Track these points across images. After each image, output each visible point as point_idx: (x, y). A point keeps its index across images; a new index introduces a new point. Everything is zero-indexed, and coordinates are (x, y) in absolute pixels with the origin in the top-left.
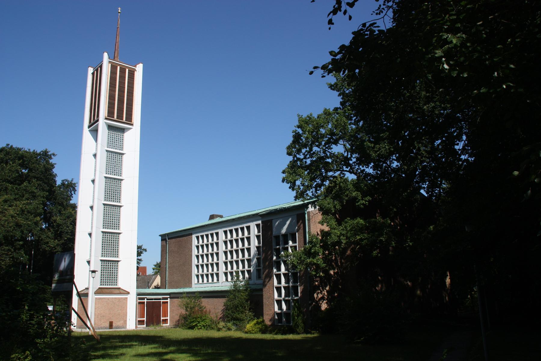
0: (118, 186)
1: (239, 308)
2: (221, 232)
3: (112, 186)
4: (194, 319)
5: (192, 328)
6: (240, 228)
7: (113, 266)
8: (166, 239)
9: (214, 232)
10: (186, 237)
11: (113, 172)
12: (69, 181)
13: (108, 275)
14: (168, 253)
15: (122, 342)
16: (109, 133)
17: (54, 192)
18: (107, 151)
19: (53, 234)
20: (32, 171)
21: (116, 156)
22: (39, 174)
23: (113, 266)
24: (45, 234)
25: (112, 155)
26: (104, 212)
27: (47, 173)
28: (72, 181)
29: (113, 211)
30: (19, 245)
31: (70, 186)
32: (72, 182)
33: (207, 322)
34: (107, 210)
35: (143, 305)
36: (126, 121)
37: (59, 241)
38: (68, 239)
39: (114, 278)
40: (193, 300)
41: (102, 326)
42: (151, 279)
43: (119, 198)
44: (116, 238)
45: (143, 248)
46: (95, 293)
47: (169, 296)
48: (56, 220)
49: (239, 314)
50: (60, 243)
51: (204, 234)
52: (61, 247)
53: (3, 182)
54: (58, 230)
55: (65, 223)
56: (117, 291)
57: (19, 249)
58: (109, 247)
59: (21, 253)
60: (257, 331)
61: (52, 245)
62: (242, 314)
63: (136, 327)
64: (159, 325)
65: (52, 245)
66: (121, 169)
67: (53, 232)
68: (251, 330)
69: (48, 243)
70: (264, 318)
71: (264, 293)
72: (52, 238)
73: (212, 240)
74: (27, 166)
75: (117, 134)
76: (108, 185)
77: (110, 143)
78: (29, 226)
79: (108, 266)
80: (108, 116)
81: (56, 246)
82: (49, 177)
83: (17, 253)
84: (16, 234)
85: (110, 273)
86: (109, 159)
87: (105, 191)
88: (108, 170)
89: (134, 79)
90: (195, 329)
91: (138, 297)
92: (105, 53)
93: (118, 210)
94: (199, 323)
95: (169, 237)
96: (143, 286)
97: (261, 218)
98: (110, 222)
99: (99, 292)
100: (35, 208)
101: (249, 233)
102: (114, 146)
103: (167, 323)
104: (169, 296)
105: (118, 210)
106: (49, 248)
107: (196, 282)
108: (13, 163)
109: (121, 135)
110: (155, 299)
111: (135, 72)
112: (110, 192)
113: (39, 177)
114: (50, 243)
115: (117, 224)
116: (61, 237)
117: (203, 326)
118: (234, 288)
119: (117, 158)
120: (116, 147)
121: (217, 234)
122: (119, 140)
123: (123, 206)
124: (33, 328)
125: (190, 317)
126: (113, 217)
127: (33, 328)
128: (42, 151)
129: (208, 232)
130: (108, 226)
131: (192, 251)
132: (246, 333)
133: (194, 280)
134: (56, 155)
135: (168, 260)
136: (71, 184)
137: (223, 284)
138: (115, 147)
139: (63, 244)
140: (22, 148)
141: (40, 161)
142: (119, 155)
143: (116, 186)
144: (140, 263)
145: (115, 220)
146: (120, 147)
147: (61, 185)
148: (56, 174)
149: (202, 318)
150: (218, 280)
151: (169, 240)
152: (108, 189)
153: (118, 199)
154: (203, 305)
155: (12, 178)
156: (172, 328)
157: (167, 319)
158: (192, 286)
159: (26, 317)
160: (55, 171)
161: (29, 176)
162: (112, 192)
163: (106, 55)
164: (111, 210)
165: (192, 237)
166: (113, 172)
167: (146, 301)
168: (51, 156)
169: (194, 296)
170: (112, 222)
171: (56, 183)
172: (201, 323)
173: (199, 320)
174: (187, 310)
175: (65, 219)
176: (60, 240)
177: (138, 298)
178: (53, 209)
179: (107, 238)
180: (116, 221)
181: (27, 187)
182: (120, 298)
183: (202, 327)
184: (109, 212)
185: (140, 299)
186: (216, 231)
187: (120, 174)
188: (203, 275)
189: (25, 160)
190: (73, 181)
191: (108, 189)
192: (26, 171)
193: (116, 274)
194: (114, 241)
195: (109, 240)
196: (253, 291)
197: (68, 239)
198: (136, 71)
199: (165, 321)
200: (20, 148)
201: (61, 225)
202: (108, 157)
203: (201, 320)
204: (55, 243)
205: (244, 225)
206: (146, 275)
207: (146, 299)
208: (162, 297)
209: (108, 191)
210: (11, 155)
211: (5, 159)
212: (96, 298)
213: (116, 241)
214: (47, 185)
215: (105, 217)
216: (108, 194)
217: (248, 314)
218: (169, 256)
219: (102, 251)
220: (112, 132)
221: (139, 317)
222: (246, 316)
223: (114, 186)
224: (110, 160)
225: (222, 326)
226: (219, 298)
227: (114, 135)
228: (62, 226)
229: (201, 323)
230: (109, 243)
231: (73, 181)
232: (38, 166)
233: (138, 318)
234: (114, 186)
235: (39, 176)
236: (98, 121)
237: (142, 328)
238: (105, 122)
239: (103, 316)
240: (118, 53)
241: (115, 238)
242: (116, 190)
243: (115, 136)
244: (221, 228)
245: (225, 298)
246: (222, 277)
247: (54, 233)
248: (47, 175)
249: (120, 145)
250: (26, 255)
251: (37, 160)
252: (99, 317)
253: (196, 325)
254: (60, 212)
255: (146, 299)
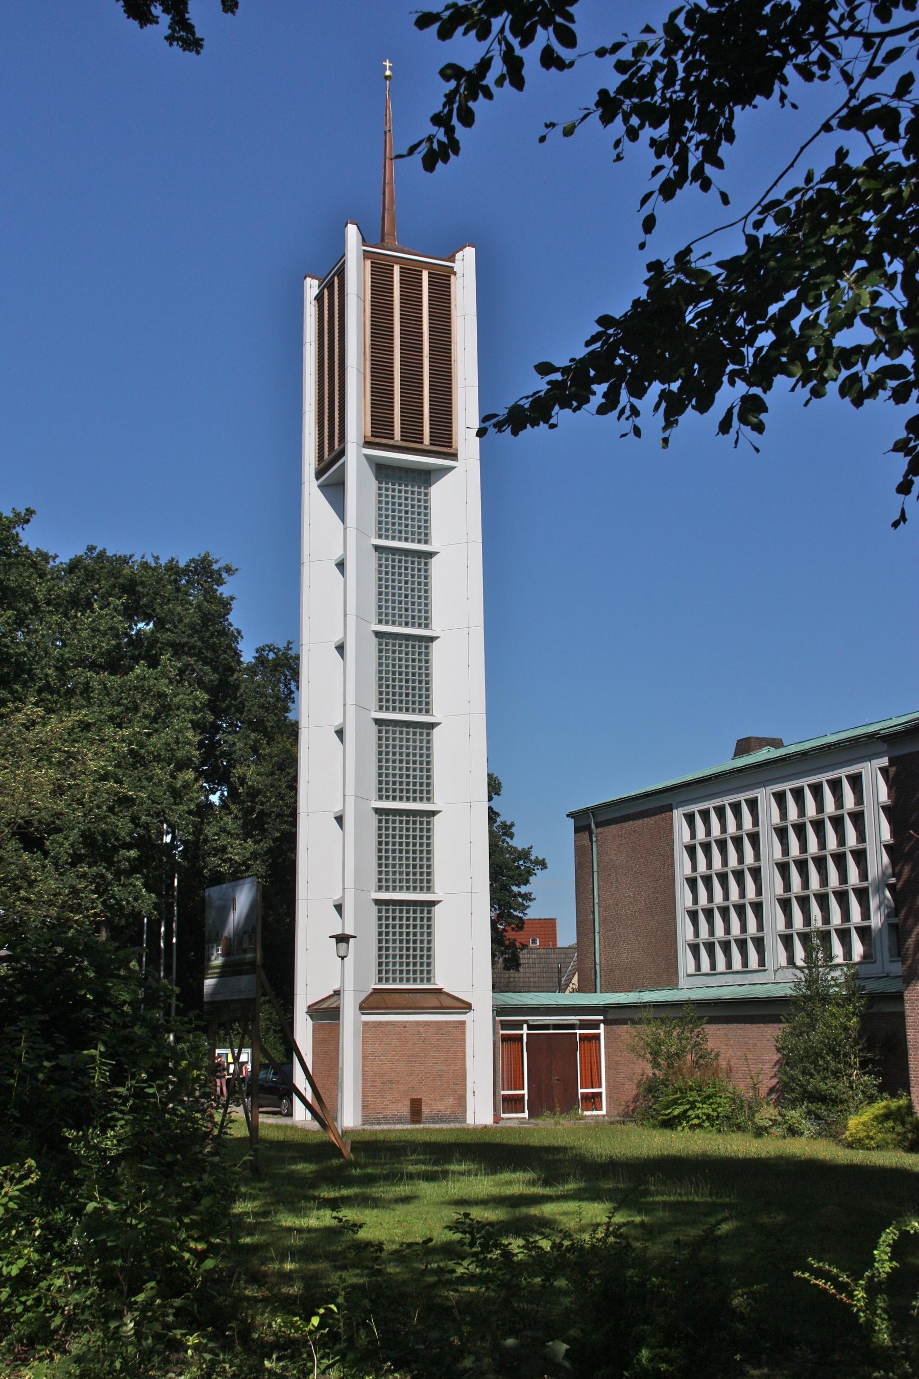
0: (420, 661)
1: (823, 1058)
2: (764, 796)
3: (400, 659)
4: (678, 1095)
5: (669, 1124)
6: (827, 781)
7: (415, 919)
8: (590, 825)
9: (741, 797)
10: (653, 818)
11: (400, 616)
12: (279, 650)
13: (401, 949)
14: (598, 871)
15: (436, 1163)
16: (380, 489)
17: (237, 687)
18: (377, 548)
19: (240, 822)
20: (163, 627)
21: (406, 562)
22: (184, 633)
23: (415, 919)
24: (214, 822)
25: (393, 560)
26: (380, 746)
27: (208, 630)
28: (288, 648)
29: (408, 740)
30: (128, 859)
31: (283, 666)
32: (290, 652)
33: (720, 1105)
34: (387, 739)
35: (516, 1045)
36: (431, 444)
37: (256, 842)
38: (283, 834)
39: (422, 957)
40: (674, 1028)
41: (389, 1113)
42: (568, 960)
43: (424, 699)
44: (421, 830)
45: (533, 858)
46: (361, 1008)
47: (601, 1018)
48: (245, 775)
49: (826, 1078)
50: (262, 848)
51: (709, 805)
52: (264, 861)
53: (75, 667)
54: (252, 810)
55: (272, 786)
56: (433, 1001)
57: (129, 873)
58: (401, 859)
59: (134, 886)
60: (883, 1139)
61: (237, 857)
62: (838, 1078)
63: (497, 1119)
64: (572, 1113)
65: (237, 857)
66: (426, 605)
67: (240, 815)
68: (862, 1134)
69: (224, 849)
70: (913, 1097)
71: (907, 1006)
72: (237, 835)
73: (737, 825)
74: (149, 611)
75: (406, 492)
76: (387, 658)
77: (387, 523)
78: (154, 802)
79: (401, 919)
80: (372, 436)
81: (249, 859)
82: (214, 643)
83: (124, 885)
84: (117, 826)
85: (408, 942)
86: (387, 573)
87: (380, 679)
88: (383, 610)
89: (448, 301)
90: (679, 1128)
91: (498, 1018)
92: (349, 226)
93: (424, 737)
94: (693, 1107)
95: (600, 819)
96: (544, 984)
97: (884, 747)
98: (401, 776)
99: (375, 1005)
100: (169, 745)
101: (859, 800)
102: (400, 532)
103: (601, 1109)
104: (601, 1018)
105: (424, 737)
106: (228, 865)
107: (691, 969)
108: (101, 608)
109: (419, 493)
110: (556, 1027)
111: (453, 277)
112: (394, 680)
113: (187, 643)
114: (230, 849)
115: (421, 784)
116: (263, 831)
117: (707, 1119)
118: (808, 988)
119: (413, 569)
120: (406, 532)
121: (753, 804)
122: (416, 509)
123: (439, 724)
124: (123, 1108)
125: (667, 1086)
126: (408, 763)
127: (123, 1108)
128: (192, 561)
129: (724, 798)
130: (394, 790)
131: (672, 865)
132: (850, 1146)
133: (686, 961)
134: (237, 570)
135: (599, 896)
136: (287, 658)
137: (780, 977)
138: (403, 535)
139: (270, 850)
140: (131, 556)
141: (187, 594)
142: (416, 559)
143: (414, 660)
144: (528, 907)
145: (414, 770)
146: (419, 534)
147: (256, 665)
148: (239, 632)
149: (701, 1091)
150: (762, 962)
151: (599, 830)
152: (387, 672)
153: (420, 703)
154: (710, 1045)
155: (102, 655)
156: (612, 1123)
157: (600, 1093)
158: (677, 984)
159: (103, 1076)
160: (235, 619)
161: (157, 641)
162: (400, 680)
163: (352, 231)
164: (401, 740)
165: (671, 818)
166: (400, 616)
167: (525, 1031)
168: (221, 575)
169: (680, 1015)
170: (408, 776)
171: (242, 659)
172: (699, 1108)
173: (692, 1096)
174: (656, 1065)
175: (273, 774)
176: (261, 840)
177: (501, 1021)
178: (234, 744)
179: (394, 829)
180: (418, 773)
181: (144, 678)
182: (442, 1022)
183: (704, 1121)
184: (394, 747)
185: (505, 1025)
186: (750, 795)
187: (423, 621)
188: (729, 942)
189: (142, 593)
190: (291, 649)
191: (387, 672)
192: (147, 624)
193: (425, 945)
194: (414, 837)
195: (401, 837)
196: (874, 998)
197: (283, 834)
198: (455, 273)
199: (593, 1101)
200: (125, 556)
201: (259, 792)
202: (383, 569)
203: (699, 1099)
204: (245, 848)
205: (843, 773)
206: (554, 947)
207: (525, 1026)
208: (580, 1020)
209: (387, 680)
210: (98, 582)
211: (82, 595)
212: (366, 1024)
213: (421, 837)
214: (212, 668)
215: (384, 763)
216: (387, 686)
217: (859, 1079)
218: (601, 883)
219: (380, 873)
220: (390, 486)
221: (506, 1087)
222: (851, 1087)
223: (407, 660)
224: (390, 576)
225: (771, 1120)
226: (764, 1023)
227: (396, 493)
228: (264, 796)
229: (699, 1108)
230: (401, 844)
231: (291, 649)
232: (179, 608)
233: (503, 1090)
234: (407, 660)
235: (185, 640)
236: (342, 453)
237: (516, 1121)
238: (366, 456)
239: (391, 1082)
240: (393, 220)
241: (418, 830)
242: (414, 674)
243: (400, 498)
244: (764, 784)
245: (780, 1022)
246: (777, 954)
247: (240, 818)
248: (208, 634)
249: (419, 527)
250: (149, 891)
251: (178, 590)
252: (378, 1083)
253: (684, 1115)
254: (255, 749)
255: (525, 1026)
